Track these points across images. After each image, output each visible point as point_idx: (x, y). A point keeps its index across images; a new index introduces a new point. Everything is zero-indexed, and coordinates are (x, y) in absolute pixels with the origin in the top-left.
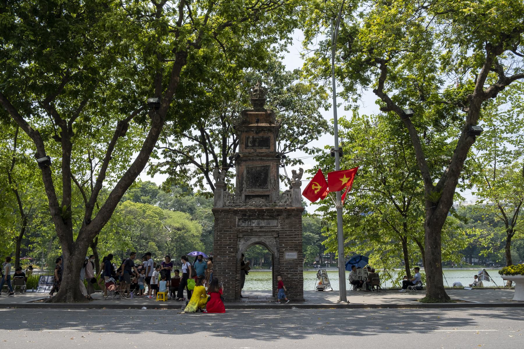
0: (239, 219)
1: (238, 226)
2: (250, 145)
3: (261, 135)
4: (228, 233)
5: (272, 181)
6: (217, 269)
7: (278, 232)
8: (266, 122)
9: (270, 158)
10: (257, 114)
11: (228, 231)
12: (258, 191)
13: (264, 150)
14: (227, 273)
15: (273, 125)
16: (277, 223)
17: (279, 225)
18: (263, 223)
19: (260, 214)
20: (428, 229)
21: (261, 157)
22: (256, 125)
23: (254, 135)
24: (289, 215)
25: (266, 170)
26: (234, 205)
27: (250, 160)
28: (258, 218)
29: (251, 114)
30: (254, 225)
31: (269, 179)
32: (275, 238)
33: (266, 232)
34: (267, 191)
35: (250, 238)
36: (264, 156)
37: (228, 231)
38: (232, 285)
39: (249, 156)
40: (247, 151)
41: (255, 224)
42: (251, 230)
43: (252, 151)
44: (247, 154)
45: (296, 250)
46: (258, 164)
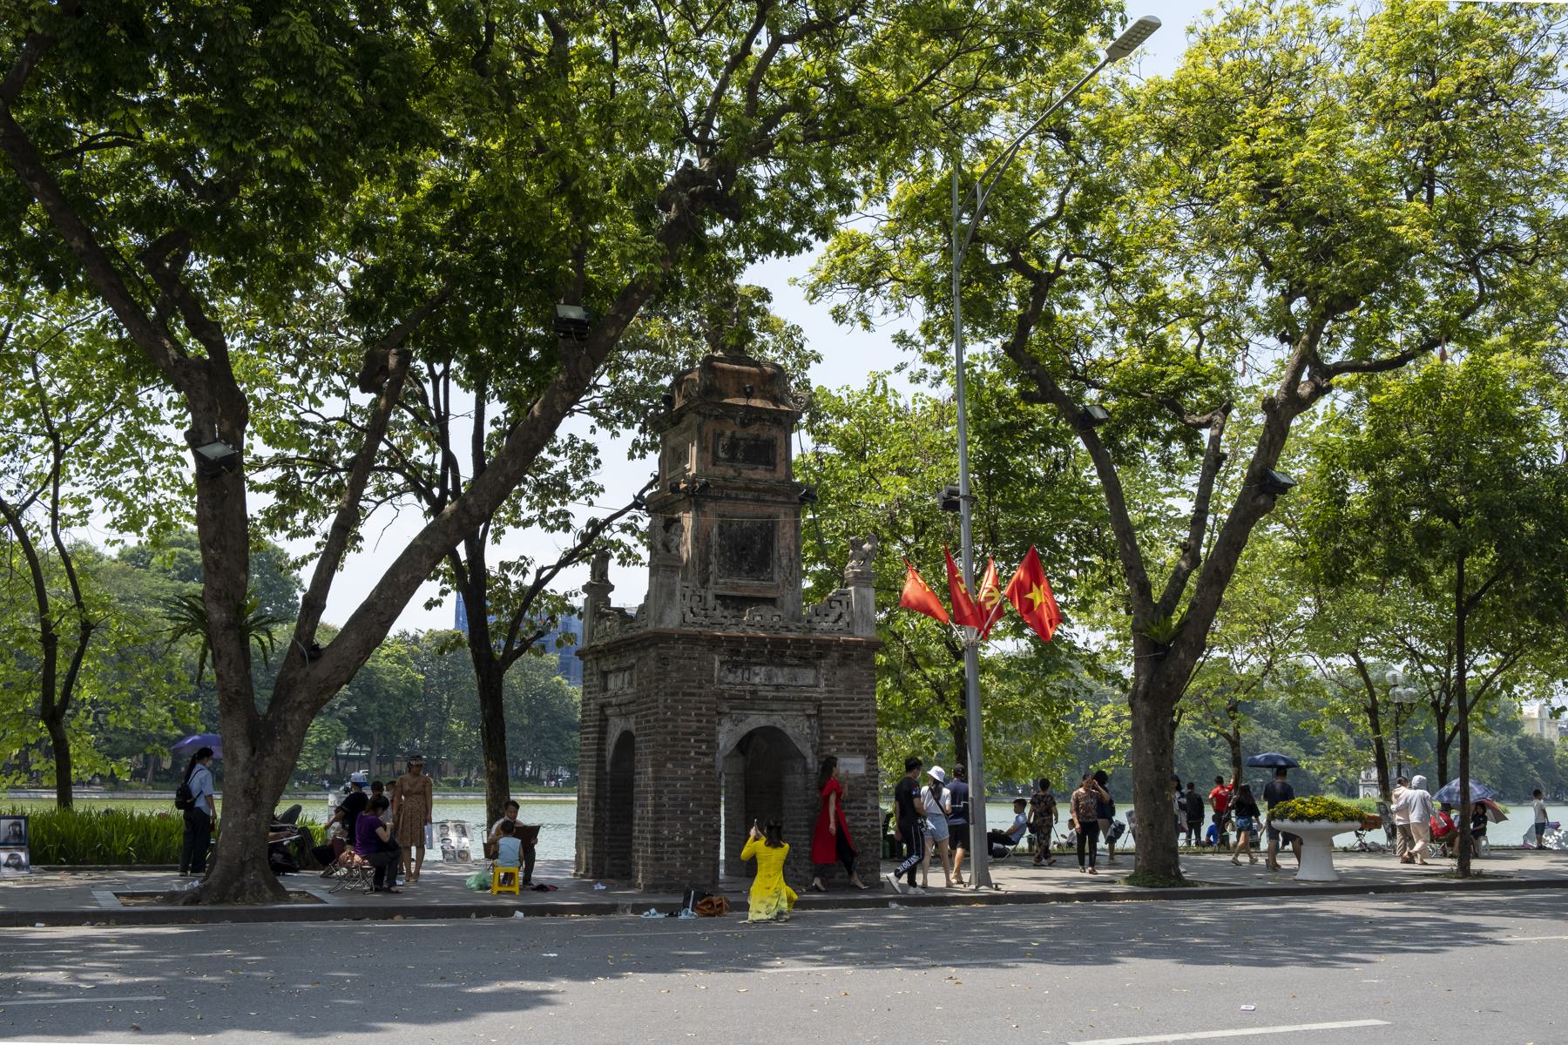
0: (722, 663)
1: (721, 682)
2: (722, 455)
3: (753, 430)
4: (694, 699)
5: (785, 562)
6: (665, 799)
7: (818, 704)
8: (763, 398)
9: (781, 499)
10: (738, 372)
11: (693, 695)
12: (748, 586)
13: (760, 474)
14: (692, 813)
15: (782, 407)
16: (816, 677)
17: (823, 683)
18: (781, 677)
19: (775, 651)
20: (1145, 708)
21: (760, 493)
22: (741, 402)
23: (735, 428)
24: (845, 657)
25: (767, 532)
26: (707, 622)
27: (728, 497)
28: (770, 662)
29: (723, 370)
30: (757, 680)
31: (776, 555)
32: (809, 716)
33: (789, 700)
34: (770, 588)
35: (747, 716)
36: (764, 491)
37: (693, 695)
38: (704, 844)
39: (726, 487)
40: (717, 471)
41: (759, 676)
42: (754, 693)
43: (731, 472)
44: (721, 482)
45: (863, 752)
46: (746, 512)
